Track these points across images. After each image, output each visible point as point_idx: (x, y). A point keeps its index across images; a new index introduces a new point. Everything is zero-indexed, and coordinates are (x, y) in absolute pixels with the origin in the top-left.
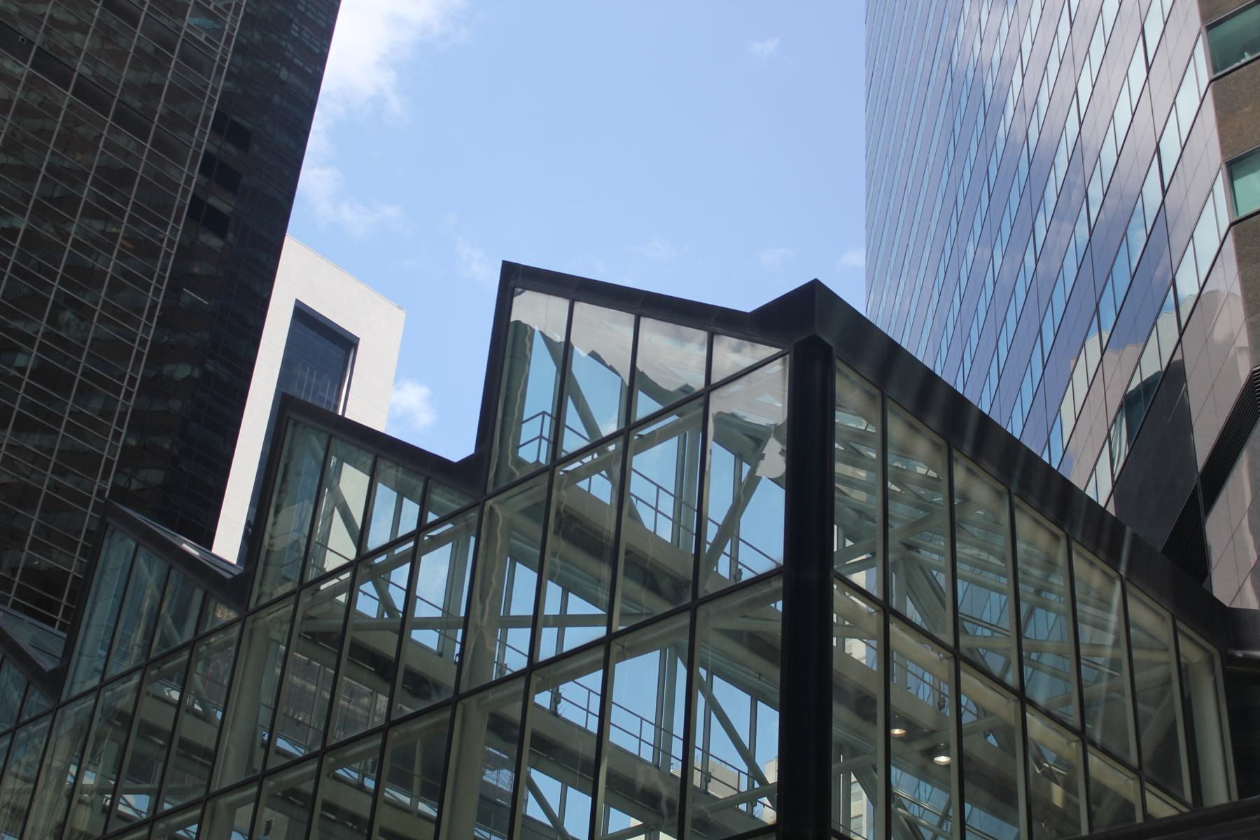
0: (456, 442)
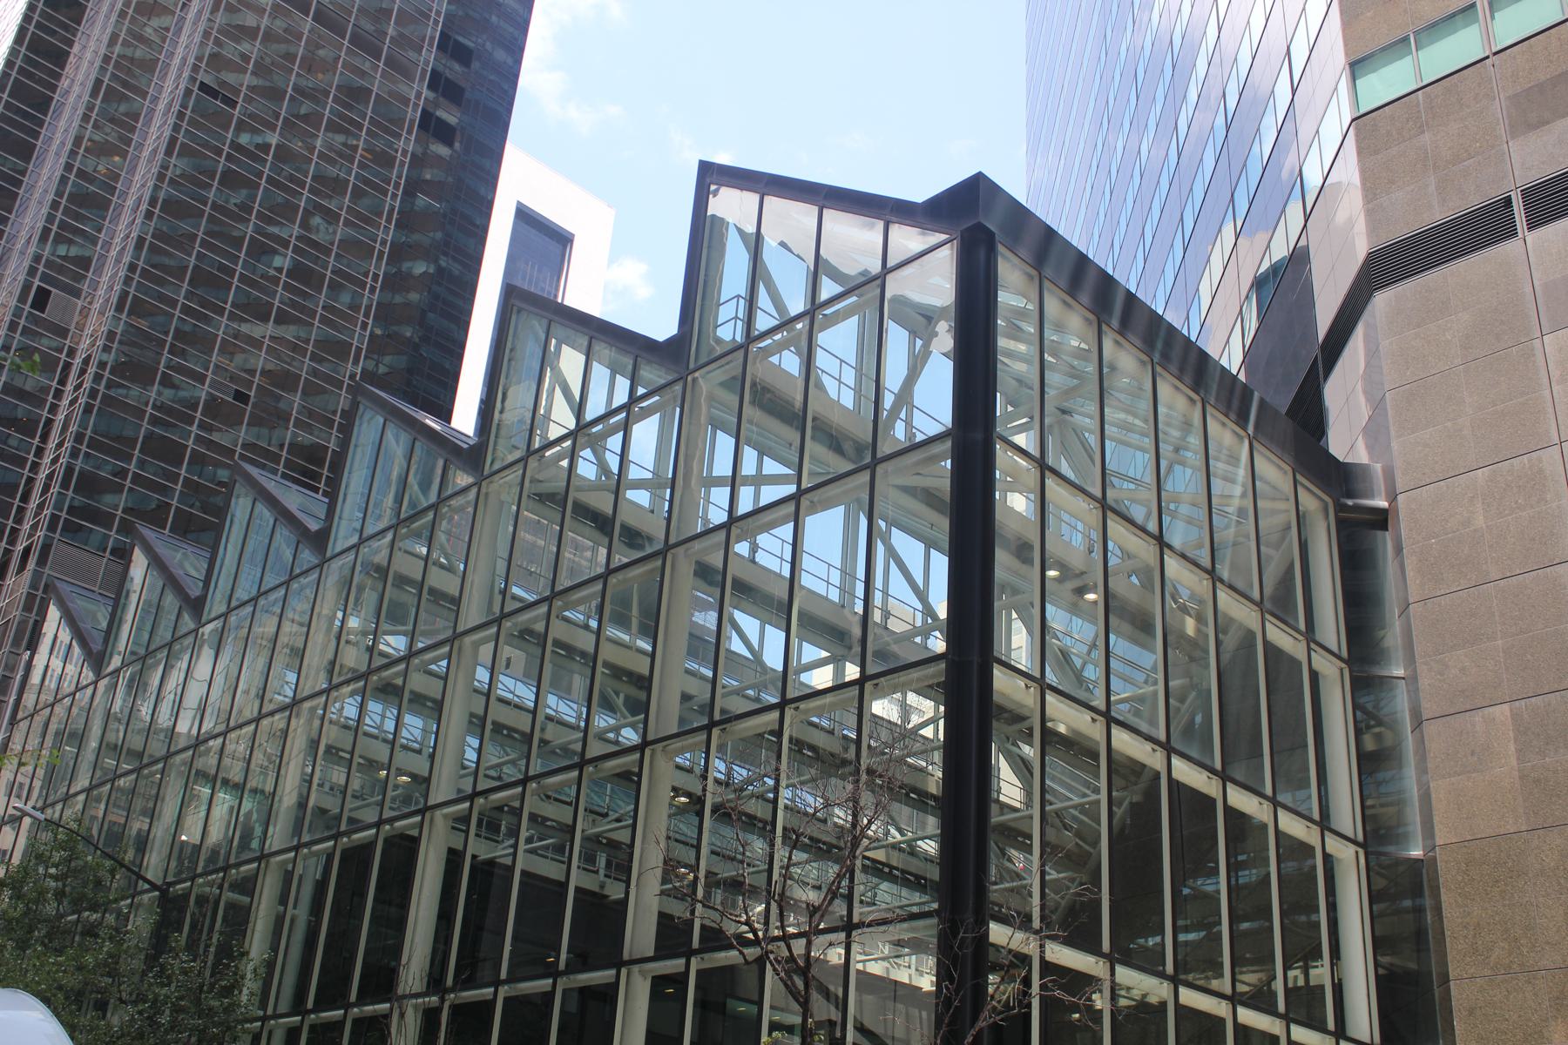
0: (662, 325)
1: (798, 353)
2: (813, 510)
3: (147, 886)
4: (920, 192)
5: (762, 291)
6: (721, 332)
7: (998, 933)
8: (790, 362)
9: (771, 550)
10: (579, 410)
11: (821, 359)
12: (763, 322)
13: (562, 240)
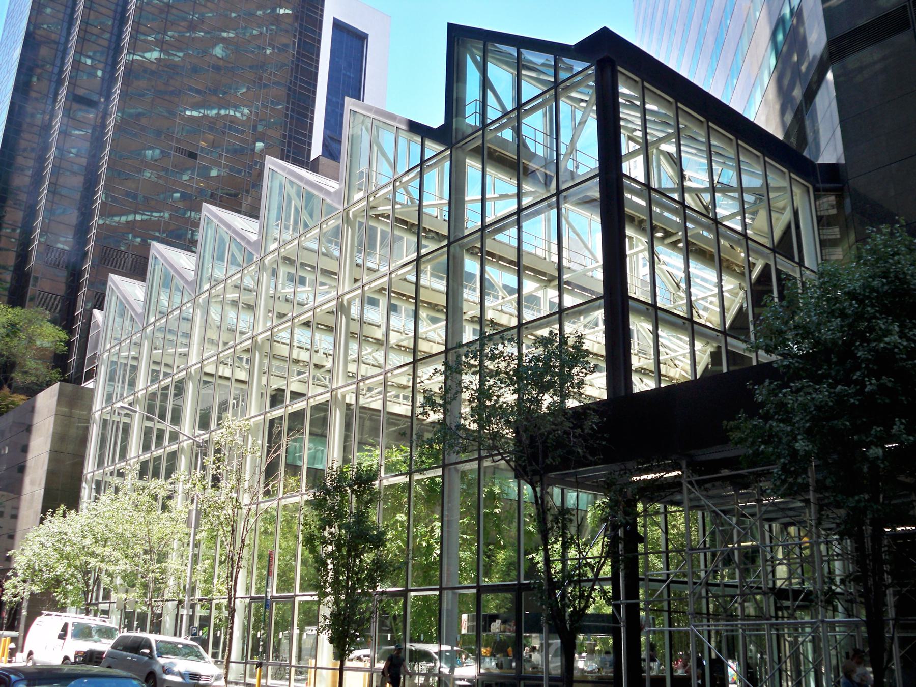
0: (435, 119)
1: (513, 129)
2: (529, 216)
3: (185, 438)
4: (572, 39)
5: (490, 94)
6: (467, 121)
7: (897, 357)
8: (508, 134)
9: (508, 237)
10: (394, 168)
11: (525, 131)
12: (492, 114)
13: (362, 37)
